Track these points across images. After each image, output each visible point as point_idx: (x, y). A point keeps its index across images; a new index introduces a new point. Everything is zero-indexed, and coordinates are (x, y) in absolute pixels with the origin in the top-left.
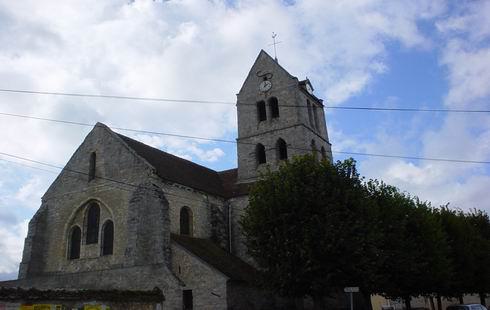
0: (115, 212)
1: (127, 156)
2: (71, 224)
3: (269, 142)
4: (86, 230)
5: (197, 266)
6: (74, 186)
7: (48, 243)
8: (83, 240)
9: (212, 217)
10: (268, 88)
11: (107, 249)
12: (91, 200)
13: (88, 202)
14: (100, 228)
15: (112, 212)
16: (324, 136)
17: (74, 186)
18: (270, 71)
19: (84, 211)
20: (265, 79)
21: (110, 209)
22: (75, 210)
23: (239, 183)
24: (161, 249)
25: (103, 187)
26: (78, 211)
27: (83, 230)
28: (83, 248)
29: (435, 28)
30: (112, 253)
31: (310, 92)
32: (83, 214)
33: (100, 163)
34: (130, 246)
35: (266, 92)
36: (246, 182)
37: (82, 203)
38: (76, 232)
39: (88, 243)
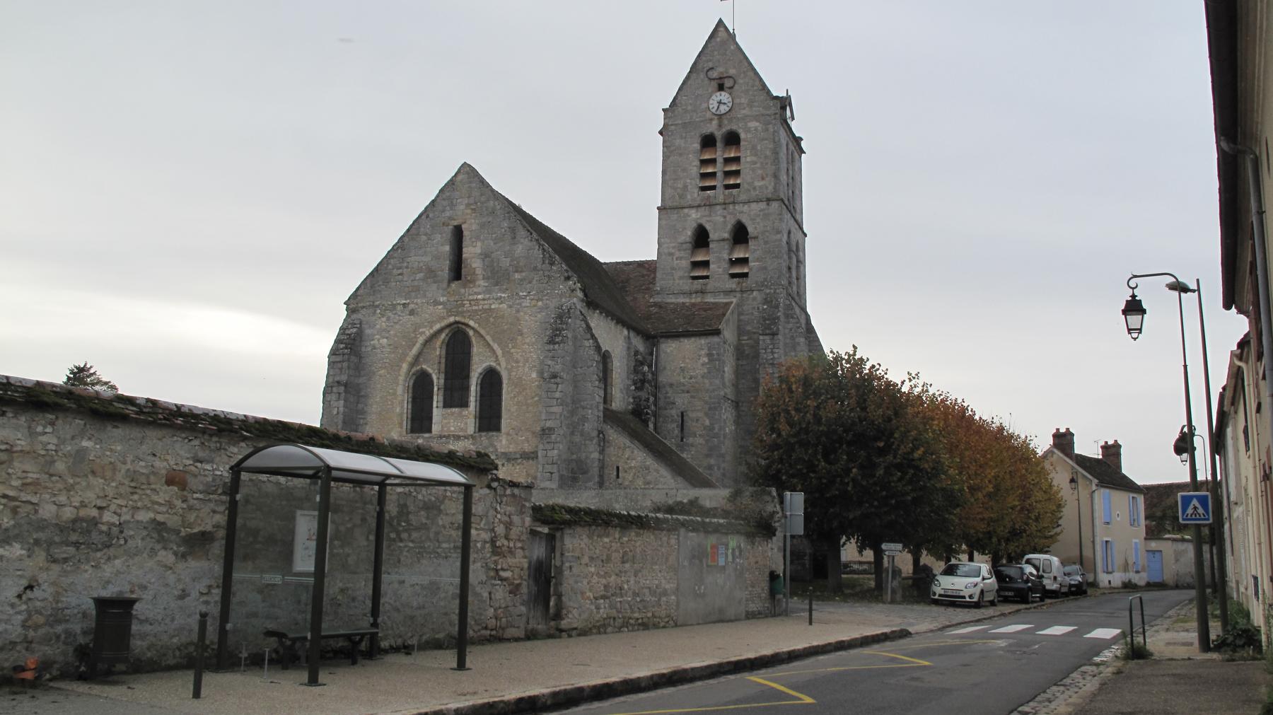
0: (507, 354)
1: (525, 246)
2: (412, 365)
3: (719, 230)
4: (442, 381)
5: (647, 468)
6: (417, 289)
7: (366, 396)
8: (437, 399)
9: (636, 371)
10: (724, 109)
11: (489, 419)
12: (457, 322)
13: (449, 325)
14: (473, 388)
15: (499, 352)
16: (798, 217)
17: (417, 289)
18: (732, 72)
19: (438, 343)
20: (721, 88)
21: (495, 346)
22: (421, 340)
23: (657, 299)
24: (595, 434)
25: (478, 293)
26: (428, 341)
27: (438, 380)
28: (437, 413)
29: (876, 585)
30: (498, 429)
31: (789, 121)
32: (438, 350)
33: (471, 251)
34: (549, 424)
35: (720, 116)
36: (672, 299)
37: (437, 326)
38: (421, 388)
39: (448, 404)
